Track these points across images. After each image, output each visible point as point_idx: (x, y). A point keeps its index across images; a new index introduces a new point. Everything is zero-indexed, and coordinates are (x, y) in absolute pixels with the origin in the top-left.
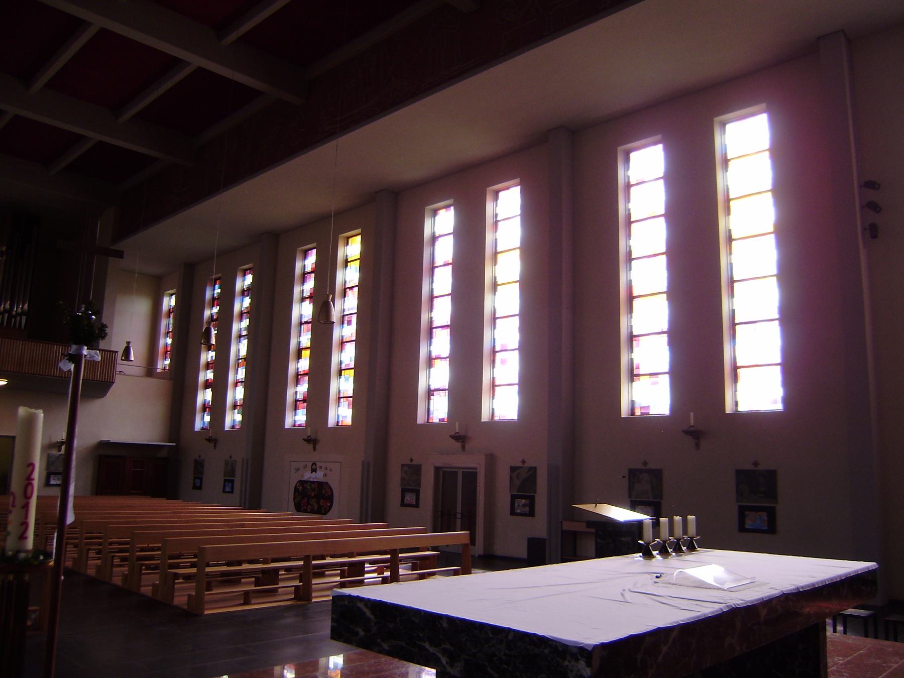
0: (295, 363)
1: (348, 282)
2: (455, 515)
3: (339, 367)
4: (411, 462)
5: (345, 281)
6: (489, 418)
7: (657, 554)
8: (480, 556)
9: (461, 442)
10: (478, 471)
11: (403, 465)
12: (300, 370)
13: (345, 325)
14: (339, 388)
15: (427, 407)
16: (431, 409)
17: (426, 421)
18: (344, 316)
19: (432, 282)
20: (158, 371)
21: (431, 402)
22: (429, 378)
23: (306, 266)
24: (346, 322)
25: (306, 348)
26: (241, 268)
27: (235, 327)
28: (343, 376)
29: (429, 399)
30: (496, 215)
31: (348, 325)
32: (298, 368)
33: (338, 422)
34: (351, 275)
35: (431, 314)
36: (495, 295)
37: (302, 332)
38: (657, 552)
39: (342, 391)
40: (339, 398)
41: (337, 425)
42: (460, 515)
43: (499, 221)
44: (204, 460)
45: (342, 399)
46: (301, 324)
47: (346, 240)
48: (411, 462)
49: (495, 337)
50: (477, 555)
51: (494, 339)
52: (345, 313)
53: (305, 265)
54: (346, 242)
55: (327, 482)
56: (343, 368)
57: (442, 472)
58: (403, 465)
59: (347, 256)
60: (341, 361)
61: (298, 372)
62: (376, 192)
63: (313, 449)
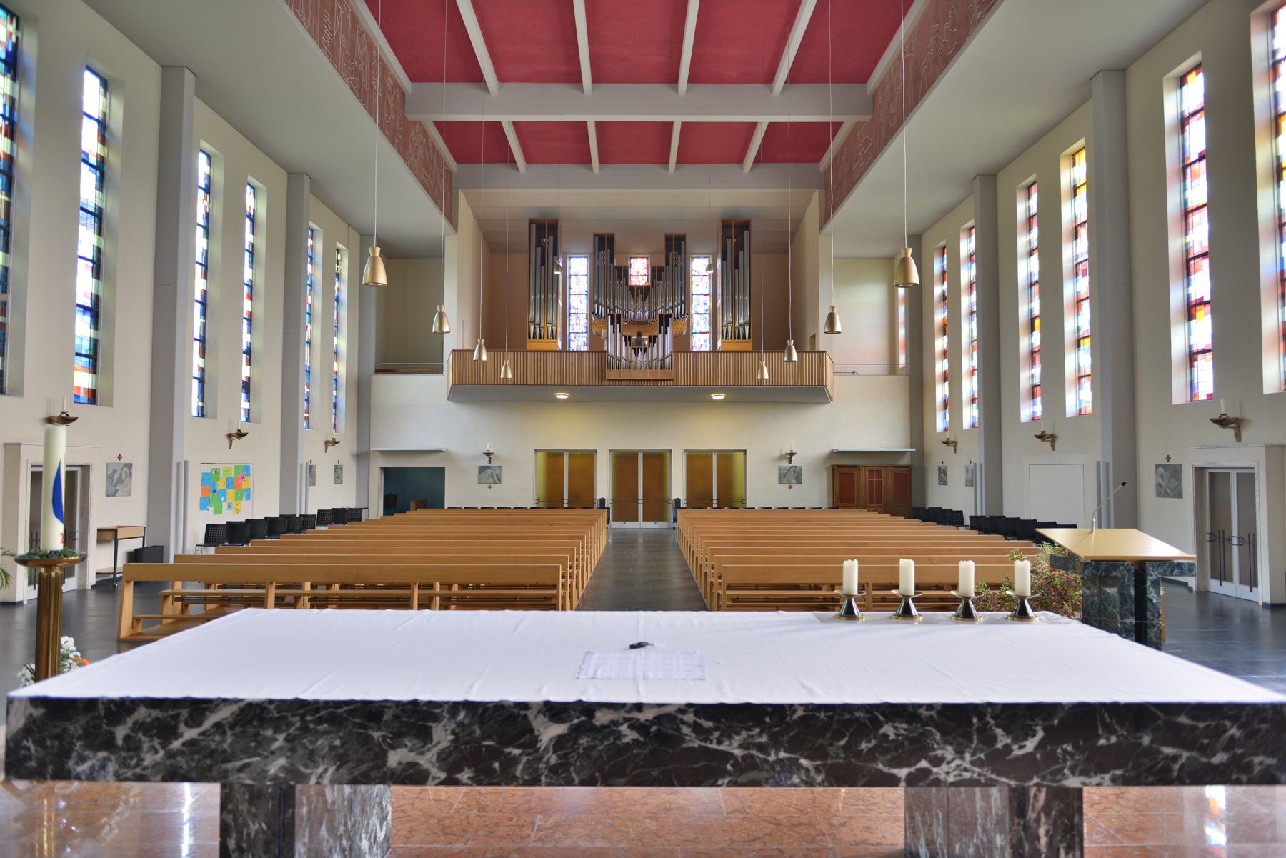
0: (1027, 337)
1: (1078, 216)
2: (1230, 540)
3: (1076, 335)
4: (1168, 461)
5: (1075, 216)
6: (1280, 388)
7: (1034, 413)
8: (1265, 605)
9: (1235, 428)
10: (1256, 471)
11: (1157, 466)
12: (1034, 347)
13: (1080, 277)
14: (1079, 364)
15: (1188, 379)
16: (1195, 381)
17: (1189, 399)
18: (1077, 265)
19: (1185, 190)
20: (901, 366)
21: (1195, 370)
22: (1189, 335)
23: (1031, 207)
24: (1080, 273)
25: (1204, 351)
26: (963, 227)
27: (1069, 326)
28: (1082, 348)
29: (1191, 366)
30: (1274, 53)
31: (1083, 277)
32: (1032, 344)
33: (1080, 410)
34: (1075, 209)
35: (1185, 239)
36: (1279, 186)
37: (1033, 295)
38: (1039, 414)
39: (1082, 368)
40: (1080, 378)
41: (1080, 414)
42: (1237, 539)
43: (1280, 61)
44: (946, 467)
45: (1083, 379)
46: (1031, 285)
47: (1071, 158)
48: (1168, 461)
49: (1284, 255)
50: (1260, 603)
51: (1282, 259)
52: (1079, 260)
53: (1029, 207)
54: (1072, 161)
55: (196, 94)
56: (1082, 336)
57: (1207, 474)
58: (1157, 466)
59: (1074, 180)
60: (1078, 327)
61: (1032, 350)
62: (1091, 79)
63: (1051, 448)
